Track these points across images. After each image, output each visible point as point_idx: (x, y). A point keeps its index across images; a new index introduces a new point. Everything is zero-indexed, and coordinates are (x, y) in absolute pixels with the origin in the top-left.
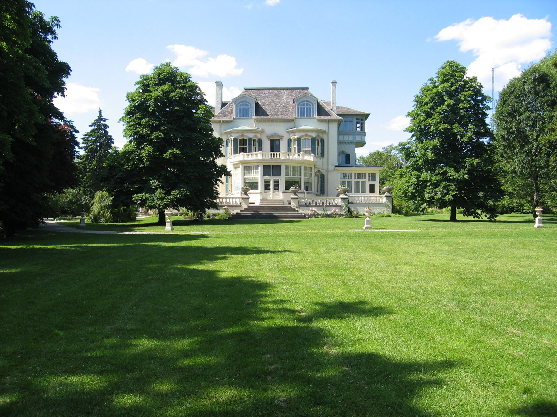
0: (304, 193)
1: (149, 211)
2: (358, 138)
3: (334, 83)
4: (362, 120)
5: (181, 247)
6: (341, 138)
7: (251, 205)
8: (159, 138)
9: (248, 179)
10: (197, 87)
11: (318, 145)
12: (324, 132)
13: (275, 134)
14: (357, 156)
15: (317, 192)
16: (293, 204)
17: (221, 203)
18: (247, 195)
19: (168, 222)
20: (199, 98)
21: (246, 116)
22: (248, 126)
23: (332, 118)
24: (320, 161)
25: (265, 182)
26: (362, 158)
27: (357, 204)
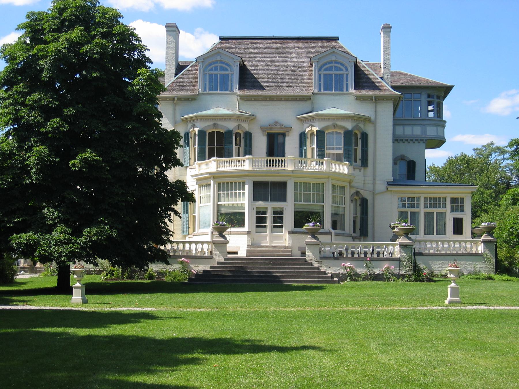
0: (329, 233)
1: (38, 265)
2: (431, 131)
3: (387, 28)
4: (439, 97)
5: (105, 337)
6: (400, 131)
7: (230, 256)
8: (60, 132)
9: (224, 206)
10: (133, 34)
11: (356, 144)
12: (367, 120)
13: (276, 123)
14: (428, 164)
15: (354, 232)
16: (310, 255)
17: (175, 251)
18: (224, 237)
19: (77, 288)
20: (136, 55)
21: (221, 89)
22: (224, 107)
23: (382, 93)
24: (359, 174)
25: (257, 213)
26: (435, 170)
27: (429, 255)
